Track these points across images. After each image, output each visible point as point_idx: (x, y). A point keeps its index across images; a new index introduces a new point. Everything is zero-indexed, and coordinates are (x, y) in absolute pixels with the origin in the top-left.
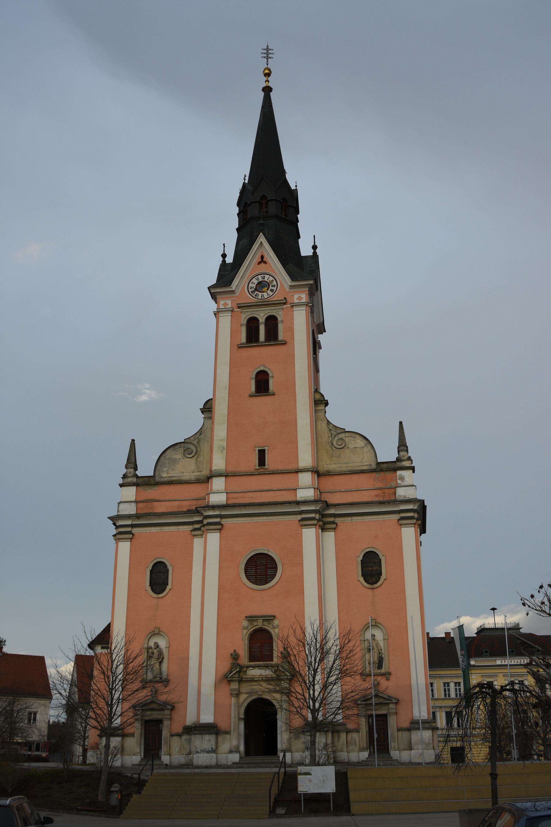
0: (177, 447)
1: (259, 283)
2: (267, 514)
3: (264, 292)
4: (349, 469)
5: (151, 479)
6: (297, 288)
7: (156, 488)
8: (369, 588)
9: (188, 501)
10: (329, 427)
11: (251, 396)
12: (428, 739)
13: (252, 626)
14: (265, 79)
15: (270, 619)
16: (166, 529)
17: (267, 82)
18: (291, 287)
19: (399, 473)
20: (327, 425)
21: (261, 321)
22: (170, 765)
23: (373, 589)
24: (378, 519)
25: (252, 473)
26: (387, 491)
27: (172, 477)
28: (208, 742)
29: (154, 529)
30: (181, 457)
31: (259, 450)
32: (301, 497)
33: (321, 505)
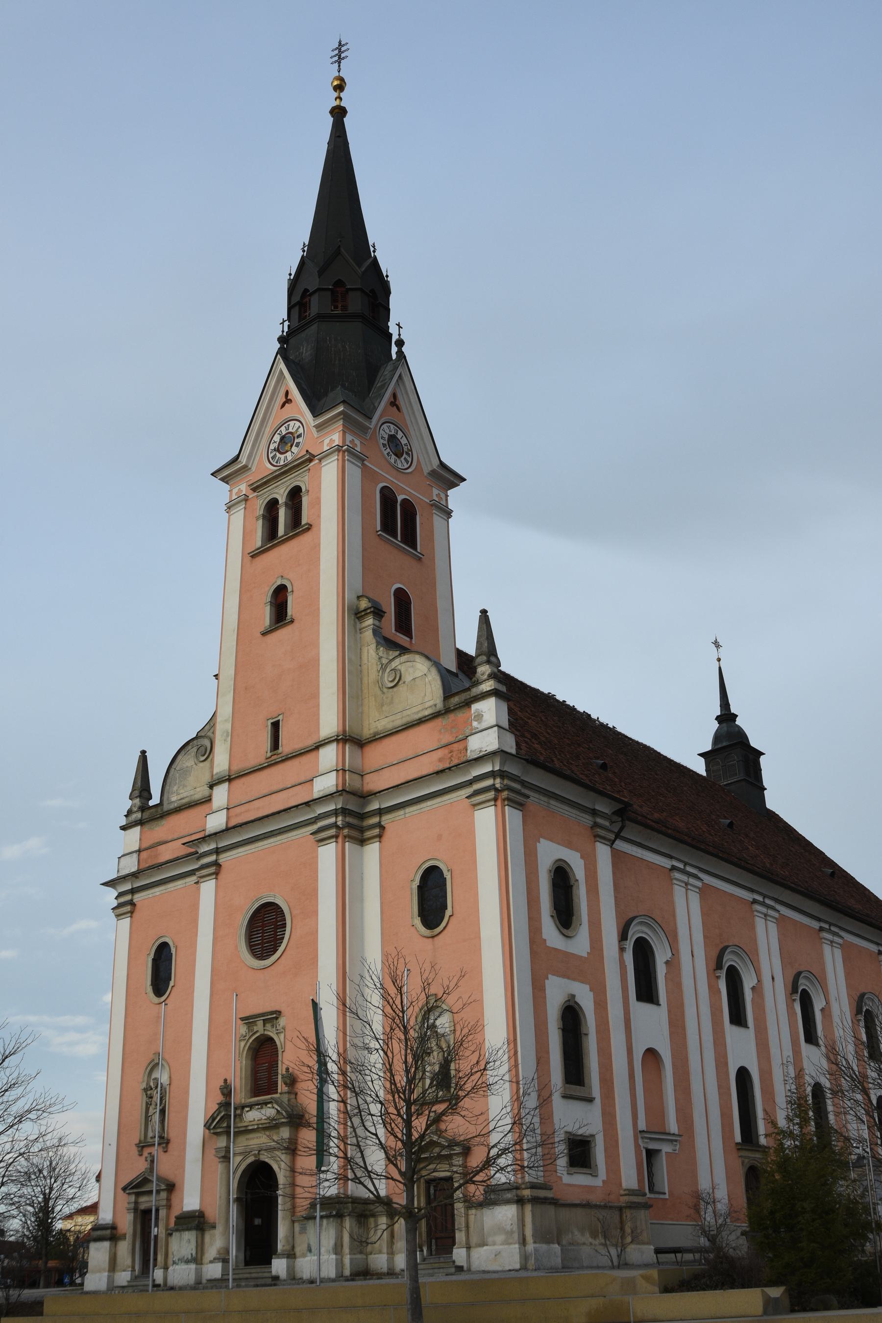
0: (190, 747)
1: (283, 438)
3: (287, 451)
4: (404, 721)
5: (159, 809)
6: (326, 427)
8: (428, 937)
11: (264, 634)
12: (510, 1222)
13: (251, 1034)
14: (336, 94)
15: (273, 1017)
16: (171, 886)
17: (338, 100)
18: (319, 427)
19: (475, 707)
23: (433, 937)
25: (260, 767)
26: (455, 745)
28: (187, 1245)
29: (157, 891)
30: (193, 763)
31: (272, 723)
32: (318, 791)
33: (341, 798)
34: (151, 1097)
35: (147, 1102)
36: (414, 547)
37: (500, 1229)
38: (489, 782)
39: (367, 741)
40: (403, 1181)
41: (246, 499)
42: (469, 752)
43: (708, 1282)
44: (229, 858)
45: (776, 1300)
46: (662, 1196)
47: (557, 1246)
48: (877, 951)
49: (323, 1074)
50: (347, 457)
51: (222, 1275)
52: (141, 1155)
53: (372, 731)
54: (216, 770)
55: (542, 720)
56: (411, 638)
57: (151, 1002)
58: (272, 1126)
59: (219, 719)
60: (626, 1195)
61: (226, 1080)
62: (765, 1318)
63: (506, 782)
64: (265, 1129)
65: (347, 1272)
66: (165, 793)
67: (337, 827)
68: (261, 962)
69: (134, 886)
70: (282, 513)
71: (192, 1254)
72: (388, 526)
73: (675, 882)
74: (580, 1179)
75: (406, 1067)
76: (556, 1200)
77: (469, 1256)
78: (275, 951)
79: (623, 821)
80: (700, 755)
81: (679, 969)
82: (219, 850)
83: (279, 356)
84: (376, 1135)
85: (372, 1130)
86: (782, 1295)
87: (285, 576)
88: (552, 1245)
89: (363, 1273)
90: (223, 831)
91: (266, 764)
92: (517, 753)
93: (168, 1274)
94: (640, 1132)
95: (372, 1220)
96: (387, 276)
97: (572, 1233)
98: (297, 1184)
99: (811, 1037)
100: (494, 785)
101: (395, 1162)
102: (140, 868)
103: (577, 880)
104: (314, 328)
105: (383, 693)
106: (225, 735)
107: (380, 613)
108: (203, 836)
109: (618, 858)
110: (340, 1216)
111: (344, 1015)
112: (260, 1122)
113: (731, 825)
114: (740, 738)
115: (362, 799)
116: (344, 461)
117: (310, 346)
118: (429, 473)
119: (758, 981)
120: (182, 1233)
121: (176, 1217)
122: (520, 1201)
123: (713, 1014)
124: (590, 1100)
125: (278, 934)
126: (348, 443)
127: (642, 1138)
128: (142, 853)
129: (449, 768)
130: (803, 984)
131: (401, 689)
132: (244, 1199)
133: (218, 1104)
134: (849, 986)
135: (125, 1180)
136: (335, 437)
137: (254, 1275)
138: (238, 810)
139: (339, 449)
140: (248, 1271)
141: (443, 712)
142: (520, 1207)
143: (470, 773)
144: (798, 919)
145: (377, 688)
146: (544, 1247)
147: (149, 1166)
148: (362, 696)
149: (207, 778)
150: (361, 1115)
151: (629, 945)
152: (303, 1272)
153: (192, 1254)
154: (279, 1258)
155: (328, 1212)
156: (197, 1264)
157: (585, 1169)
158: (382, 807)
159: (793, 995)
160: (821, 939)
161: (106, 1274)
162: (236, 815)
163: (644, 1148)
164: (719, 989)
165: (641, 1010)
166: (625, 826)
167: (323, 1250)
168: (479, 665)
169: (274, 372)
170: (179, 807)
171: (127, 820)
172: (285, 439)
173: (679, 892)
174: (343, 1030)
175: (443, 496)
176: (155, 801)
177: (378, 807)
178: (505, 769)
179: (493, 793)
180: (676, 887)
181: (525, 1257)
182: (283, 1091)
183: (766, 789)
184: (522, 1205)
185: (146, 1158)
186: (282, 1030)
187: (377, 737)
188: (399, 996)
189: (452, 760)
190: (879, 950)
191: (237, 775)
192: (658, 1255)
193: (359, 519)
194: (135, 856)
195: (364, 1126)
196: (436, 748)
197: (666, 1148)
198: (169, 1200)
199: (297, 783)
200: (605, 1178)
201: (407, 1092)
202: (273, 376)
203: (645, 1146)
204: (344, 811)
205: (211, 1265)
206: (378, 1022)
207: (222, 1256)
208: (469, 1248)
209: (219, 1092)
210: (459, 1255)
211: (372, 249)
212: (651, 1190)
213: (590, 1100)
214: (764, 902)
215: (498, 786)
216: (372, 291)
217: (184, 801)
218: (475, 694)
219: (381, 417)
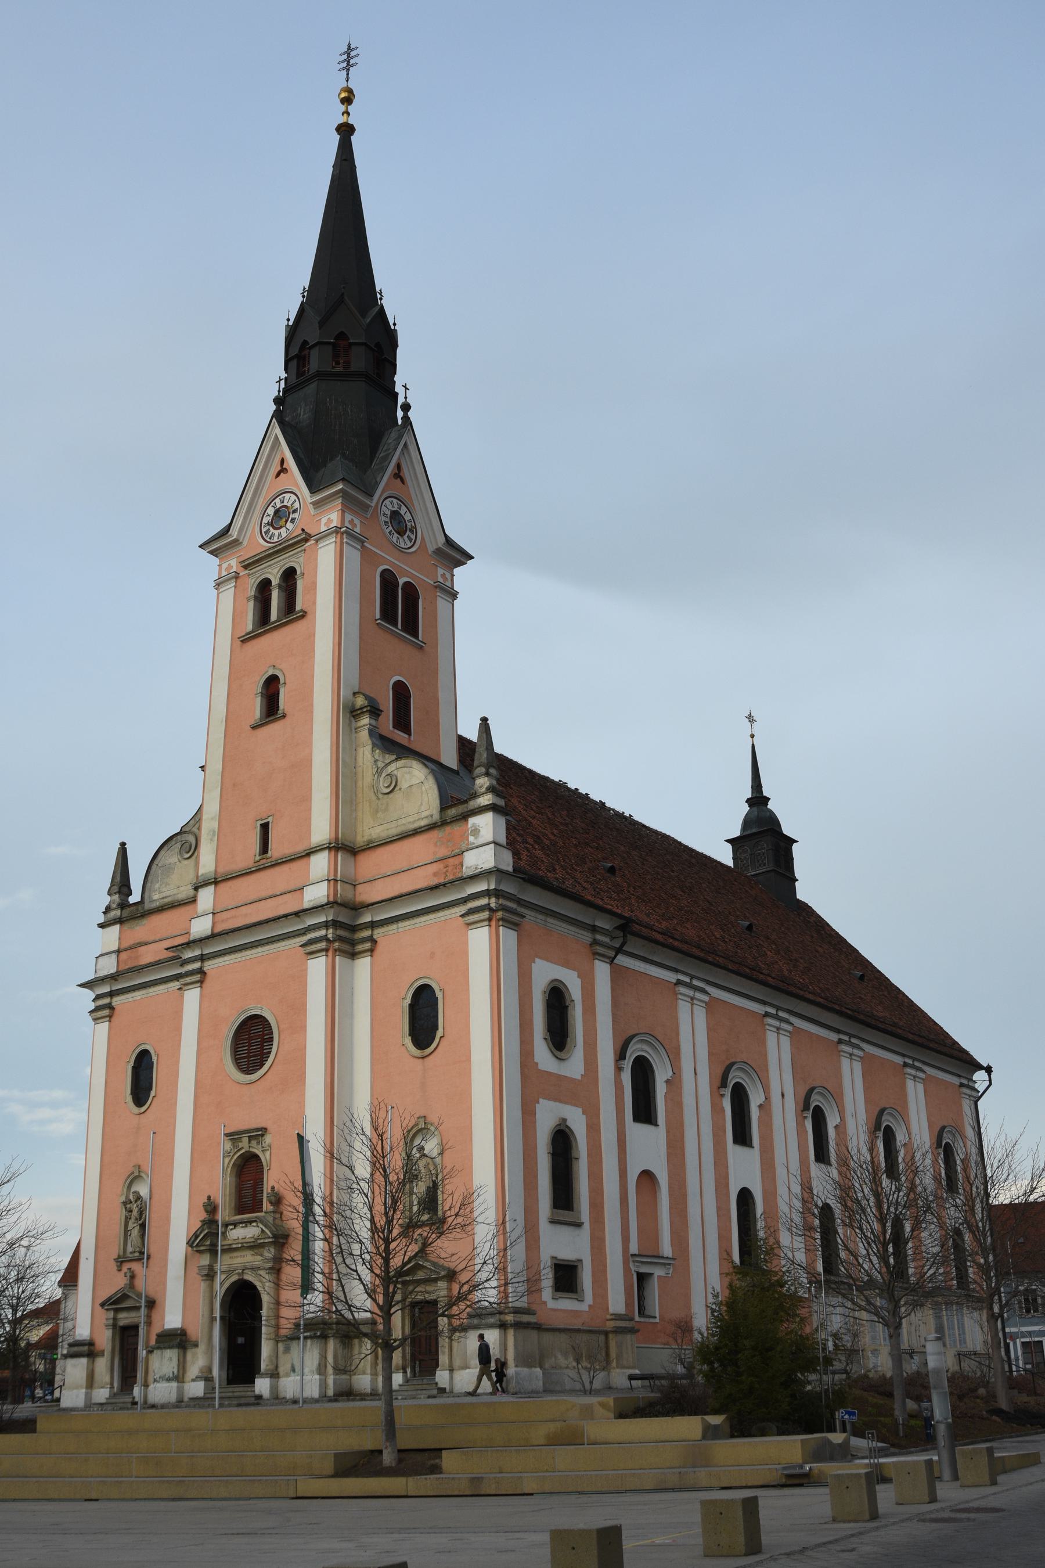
0: (173, 842)
1: (277, 512)
2: (262, 942)
3: (281, 527)
5: (140, 908)
7: (145, 921)
9: (181, 937)
10: (373, 757)
11: (254, 727)
13: (236, 1150)
14: (343, 108)
15: (258, 1134)
16: (153, 991)
17: (345, 115)
18: (316, 504)
19: (472, 821)
20: (371, 752)
21: (273, 584)
22: (145, 1402)
23: (423, 1058)
26: (450, 860)
27: (166, 897)
29: (138, 995)
30: (177, 860)
31: (261, 825)
33: (332, 910)
34: (131, 1211)
35: (126, 1216)
36: (415, 633)
38: (483, 901)
39: (360, 849)
40: (381, 1314)
41: (237, 576)
42: (464, 868)
43: (661, 1410)
44: (215, 966)
45: (716, 1427)
46: (652, 1320)
47: (538, 1369)
48: (902, 1063)
49: (309, 1212)
50: (345, 540)
51: (204, 1393)
52: (120, 1270)
53: (366, 838)
54: (201, 871)
56: (410, 734)
58: (255, 1246)
59: (205, 817)
60: (612, 1320)
61: (209, 1197)
63: (501, 901)
64: (250, 1248)
65: (330, 1392)
67: (328, 940)
68: (247, 1076)
69: (113, 989)
70: (275, 595)
71: (173, 1372)
72: (388, 613)
73: (680, 996)
74: (566, 1304)
76: (539, 1324)
77: (451, 1378)
78: (262, 1065)
79: (624, 936)
82: (205, 957)
83: (274, 420)
84: (356, 1271)
85: (353, 1267)
87: (277, 666)
88: (533, 1369)
89: (347, 1394)
90: (207, 938)
91: (254, 869)
92: (514, 870)
93: (148, 1392)
94: (632, 1255)
95: (356, 1341)
96: (395, 324)
97: (556, 1357)
98: (282, 1316)
101: (373, 1296)
104: (312, 387)
105: (378, 799)
107: (377, 712)
109: (618, 975)
110: (324, 1337)
111: (332, 1162)
113: (750, 928)
114: (773, 823)
116: (342, 543)
118: (434, 552)
122: (503, 1326)
124: (579, 1225)
126: (347, 524)
127: (633, 1261)
129: (444, 885)
130: (816, 1100)
134: (867, 1100)
135: (105, 1294)
136: (332, 517)
137: (236, 1394)
138: (225, 915)
139: (337, 531)
140: (231, 1390)
141: (439, 824)
143: (465, 890)
144: (814, 1032)
146: (525, 1371)
147: (128, 1282)
148: (356, 801)
149: (190, 878)
150: (342, 1254)
151: (628, 1065)
152: (286, 1391)
153: (173, 1372)
154: (262, 1378)
155: (312, 1333)
156: (178, 1382)
157: (570, 1294)
160: (840, 1051)
161: (84, 1390)
162: (223, 921)
163: (635, 1271)
164: (723, 1108)
165: (637, 1132)
166: (626, 942)
167: (306, 1370)
168: (477, 777)
170: (162, 907)
172: (280, 513)
173: (683, 1008)
174: (331, 1179)
175: (448, 576)
176: (135, 898)
177: (370, 920)
178: (501, 887)
179: (488, 913)
182: (268, 1210)
183: (797, 880)
184: (505, 1330)
185: (125, 1273)
186: (268, 1148)
187: (371, 845)
188: (380, 1142)
191: (223, 878)
193: (357, 607)
194: (114, 956)
195: (345, 1263)
196: (431, 861)
197: (658, 1272)
198: (149, 1316)
200: (591, 1303)
201: (386, 1231)
202: (267, 441)
203: (637, 1269)
204: (335, 924)
205: (193, 1384)
206: (363, 1169)
207: (205, 1375)
208: (451, 1370)
209: (202, 1208)
210: (442, 1377)
211: (379, 296)
212: (642, 1311)
213: (579, 1225)
215: (493, 905)
216: (378, 345)
217: (166, 900)
218: (472, 808)
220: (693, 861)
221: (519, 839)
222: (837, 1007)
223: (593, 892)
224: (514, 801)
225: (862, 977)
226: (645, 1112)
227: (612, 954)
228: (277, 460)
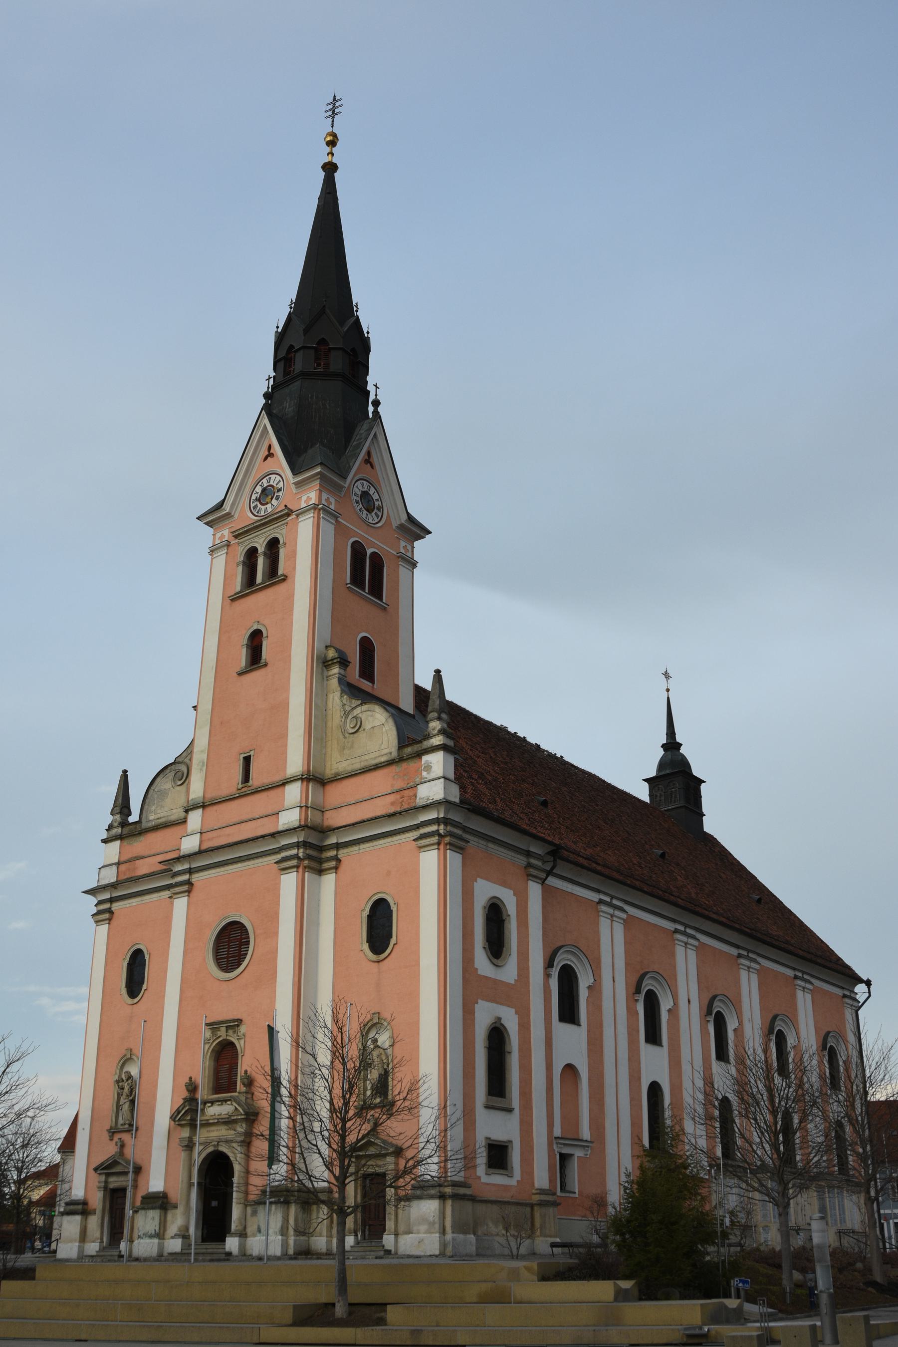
0: (168, 771)
3: (267, 503)
4: (363, 764)
7: (142, 838)
11: (240, 674)
14: (328, 149)
15: (235, 1024)
16: (147, 898)
17: (330, 155)
19: (426, 758)
22: (130, 1255)
23: (378, 962)
24: (392, 843)
25: (231, 797)
26: (406, 792)
28: (151, 1222)
29: (134, 901)
30: (171, 786)
31: (244, 758)
33: (303, 832)
34: (123, 1089)
36: (380, 598)
37: (423, 1220)
38: (434, 828)
39: (329, 780)
40: (336, 1184)
41: (228, 544)
42: (417, 798)
46: (572, 1195)
47: (472, 1236)
48: (793, 976)
50: (322, 515)
52: (111, 1140)
53: (333, 772)
54: (192, 796)
55: (491, 757)
56: (373, 682)
57: (125, 1002)
59: (196, 749)
61: (191, 1078)
62: (615, 1304)
63: (449, 828)
65: (291, 1251)
66: (144, 812)
69: (113, 896)
70: (261, 561)
71: (155, 1230)
72: (357, 579)
74: (498, 1179)
75: (343, 1092)
76: (474, 1197)
77: (396, 1241)
78: (239, 965)
79: (555, 861)
80: (644, 780)
81: (600, 992)
82: (192, 870)
84: (316, 1146)
85: (314, 1142)
86: (631, 1287)
88: (468, 1236)
89: (305, 1253)
90: (195, 854)
91: (237, 795)
94: (556, 1138)
96: (368, 333)
97: (487, 1225)
99: (722, 1055)
100: (438, 830)
102: (119, 879)
103: (509, 915)
104: (298, 384)
105: (345, 738)
106: (201, 764)
107: (346, 663)
108: (178, 856)
109: (548, 894)
110: (287, 1203)
112: (220, 1117)
113: (663, 856)
114: (684, 765)
115: (322, 834)
117: (293, 402)
118: (397, 527)
119: (675, 1004)
120: (147, 1211)
121: (142, 1197)
122: (442, 1197)
123: (630, 1034)
124: (510, 1110)
125: (242, 950)
126: (323, 502)
127: (557, 1143)
128: (121, 866)
129: (400, 813)
130: (718, 1006)
131: (361, 735)
132: (203, 1184)
133: (183, 1099)
136: (311, 496)
138: (210, 835)
139: (315, 507)
140: (204, 1247)
141: (397, 760)
142: (442, 1201)
145: (340, 733)
146: (461, 1236)
149: (182, 801)
151: (555, 972)
152: (252, 1250)
153: (155, 1230)
154: (232, 1237)
156: (159, 1239)
157: (502, 1170)
158: (340, 841)
159: (708, 1017)
160: (739, 964)
161: (77, 1244)
162: (209, 840)
164: (637, 1011)
165: (562, 1030)
167: (271, 1231)
168: (431, 720)
169: (259, 426)
170: (157, 826)
171: (107, 834)
172: (267, 491)
173: (604, 924)
175: (409, 547)
176: (134, 818)
177: (336, 842)
179: (437, 838)
180: (602, 919)
181: (444, 1245)
182: (242, 1091)
183: (705, 815)
184: (444, 1200)
185: (116, 1142)
186: (242, 1036)
187: (338, 778)
188: (340, 1034)
189: (402, 805)
190: (795, 975)
192: (553, 1249)
194: (114, 868)
195: (307, 1139)
197: (578, 1153)
198: (135, 1181)
199: (264, 814)
200: (519, 1179)
201: (343, 1111)
203: (560, 1150)
204: (305, 844)
207: (182, 1233)
208: (397, 1235)
210: (388, 1240)
211: (355, 309)
212: (563, 1187)
213: (510, 1110)
214: (685, 931)
215: (442, 831)
216: (353, 350)
219: (354, 476)
220: (615, 796)
221: (465, 775)
222: (737, 926)
223: (528, 822)
224: (462, 742)
225: (759, 901)
226: (569, 1014)
227: (543, 875)
228: (265, 446)
